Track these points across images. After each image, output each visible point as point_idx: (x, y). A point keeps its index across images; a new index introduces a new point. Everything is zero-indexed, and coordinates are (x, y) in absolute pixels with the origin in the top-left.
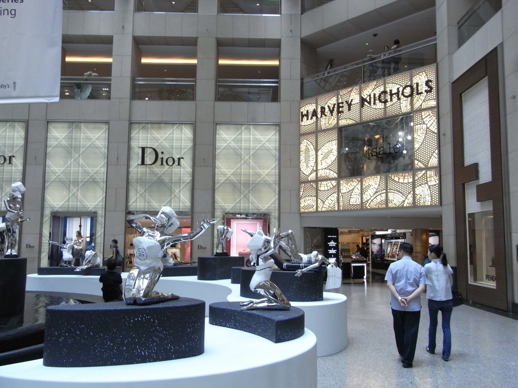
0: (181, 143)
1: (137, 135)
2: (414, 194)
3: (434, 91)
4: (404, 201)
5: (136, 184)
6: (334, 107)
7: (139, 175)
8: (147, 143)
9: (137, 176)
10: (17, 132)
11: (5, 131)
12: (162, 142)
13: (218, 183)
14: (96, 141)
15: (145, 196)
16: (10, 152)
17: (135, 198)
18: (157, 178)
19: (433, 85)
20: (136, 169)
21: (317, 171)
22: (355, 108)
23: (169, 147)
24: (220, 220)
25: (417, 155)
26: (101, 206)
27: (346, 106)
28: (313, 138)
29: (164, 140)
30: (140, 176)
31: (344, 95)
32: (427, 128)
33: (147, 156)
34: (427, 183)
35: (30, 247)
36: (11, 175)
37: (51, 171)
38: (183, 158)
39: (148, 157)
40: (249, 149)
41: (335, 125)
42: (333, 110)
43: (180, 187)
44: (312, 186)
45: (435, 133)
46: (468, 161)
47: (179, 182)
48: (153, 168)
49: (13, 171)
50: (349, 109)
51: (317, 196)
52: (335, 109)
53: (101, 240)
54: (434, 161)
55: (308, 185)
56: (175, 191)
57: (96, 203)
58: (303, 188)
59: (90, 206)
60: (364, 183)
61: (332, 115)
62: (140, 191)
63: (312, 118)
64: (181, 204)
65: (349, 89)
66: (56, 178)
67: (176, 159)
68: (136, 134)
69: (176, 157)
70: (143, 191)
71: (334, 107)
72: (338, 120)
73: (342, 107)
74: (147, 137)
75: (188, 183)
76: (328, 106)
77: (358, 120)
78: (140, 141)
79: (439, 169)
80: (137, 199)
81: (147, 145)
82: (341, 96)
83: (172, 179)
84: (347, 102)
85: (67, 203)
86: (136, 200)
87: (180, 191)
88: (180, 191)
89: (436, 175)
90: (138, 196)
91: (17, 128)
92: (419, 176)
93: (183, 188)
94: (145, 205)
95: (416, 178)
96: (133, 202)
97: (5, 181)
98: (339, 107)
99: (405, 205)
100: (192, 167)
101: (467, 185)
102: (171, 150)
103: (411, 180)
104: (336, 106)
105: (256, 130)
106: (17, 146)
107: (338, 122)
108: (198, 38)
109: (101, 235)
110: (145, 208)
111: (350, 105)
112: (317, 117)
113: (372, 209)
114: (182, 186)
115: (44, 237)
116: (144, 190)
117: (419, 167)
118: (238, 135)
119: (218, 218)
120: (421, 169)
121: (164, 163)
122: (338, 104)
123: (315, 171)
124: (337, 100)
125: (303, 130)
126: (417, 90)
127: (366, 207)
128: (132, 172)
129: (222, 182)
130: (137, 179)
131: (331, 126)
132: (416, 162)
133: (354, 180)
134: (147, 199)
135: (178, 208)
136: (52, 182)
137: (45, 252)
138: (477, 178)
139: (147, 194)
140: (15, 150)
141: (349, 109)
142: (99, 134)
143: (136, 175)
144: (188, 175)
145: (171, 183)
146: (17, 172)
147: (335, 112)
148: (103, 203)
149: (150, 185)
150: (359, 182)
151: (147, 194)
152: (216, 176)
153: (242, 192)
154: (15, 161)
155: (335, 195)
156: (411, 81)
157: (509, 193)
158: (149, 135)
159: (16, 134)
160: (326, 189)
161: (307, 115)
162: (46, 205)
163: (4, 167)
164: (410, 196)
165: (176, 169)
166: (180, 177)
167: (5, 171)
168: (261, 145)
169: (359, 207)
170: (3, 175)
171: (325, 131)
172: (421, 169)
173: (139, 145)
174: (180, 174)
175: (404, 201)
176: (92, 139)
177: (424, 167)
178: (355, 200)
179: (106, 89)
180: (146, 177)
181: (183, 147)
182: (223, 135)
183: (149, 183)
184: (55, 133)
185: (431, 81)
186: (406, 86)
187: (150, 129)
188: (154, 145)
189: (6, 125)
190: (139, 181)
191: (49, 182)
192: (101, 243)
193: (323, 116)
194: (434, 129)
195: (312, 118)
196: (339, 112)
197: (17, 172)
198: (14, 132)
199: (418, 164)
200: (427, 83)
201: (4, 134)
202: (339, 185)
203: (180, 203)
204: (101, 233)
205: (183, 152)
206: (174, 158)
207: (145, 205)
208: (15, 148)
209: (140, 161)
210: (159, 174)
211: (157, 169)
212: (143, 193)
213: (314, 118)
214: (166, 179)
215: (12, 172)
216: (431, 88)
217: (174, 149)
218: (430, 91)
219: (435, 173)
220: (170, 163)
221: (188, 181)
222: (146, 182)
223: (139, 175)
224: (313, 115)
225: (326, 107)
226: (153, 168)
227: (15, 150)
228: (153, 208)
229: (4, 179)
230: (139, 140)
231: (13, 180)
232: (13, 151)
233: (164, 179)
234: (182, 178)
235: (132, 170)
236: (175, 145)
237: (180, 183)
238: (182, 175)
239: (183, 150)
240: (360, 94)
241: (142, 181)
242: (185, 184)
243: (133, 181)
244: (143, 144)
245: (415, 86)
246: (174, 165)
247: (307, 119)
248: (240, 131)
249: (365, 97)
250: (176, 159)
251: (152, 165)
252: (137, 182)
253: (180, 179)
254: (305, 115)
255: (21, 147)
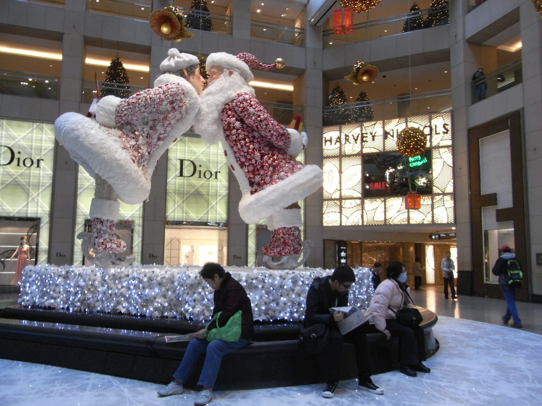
0: (218, 158)
1: (175, 147)
2: (433, 214)
3: (450, 133)
4: (424, 220)
5: (174, 195)
6: (358, 137)
7: (177, 186)
8: (185, 155)
9: (175, 187)
10: (45, 134)
11: (32, 132)
12: (199, 156)
13: (81, 188)
14: (21, 141)
15: (183, 207)
16: (38, 155)
17: (173, 209)
18: (194, 190)
19: (449, 127)
20: (174, 180)
21: (340, 190)
22: (379, 139)
23: (206, 161)
24: (82, 226)
25: (435, 183)
26: (138, 216)
27: (370, 137)
28: (336, 162)
29: (201, 154)
30: (178, 188)
31: (368, 127)
32: (444, 162)
33: (185, 168)
34: (444, 205)
35: (60, 255)
36: (39, 179)
37: (84, 178)
38: (43, 160)
39: (186, 169)
40: (217, 163)
41: (359, 152)
42: (357, 139)
43: (217, 199)
44: (336, 203)
45: (451, 167)
46: (486, 190)
47: (216, 195)
48: (190, 180)
49: (41, 175)
50: (373, 140)
51: (341, 212)
52: (359, 138)
53: (138, 249)
54: (450, 189)
55: (331, 202)
56: (32, 195)
57: (133, 212)
58: (326, 205)
59: (127, 215)
60: (387, 203)
61: (356, 143)
62: (178, 201)
63: (335, 144)
64: (39, 209)
65: (374, 123)
66: (89, 185)
67: (35, 161)
68: (173, 146)
69: (213, 171)
70: (181, 202)
71: (358, 137)
72: (362, 147)
73: (366, 137)
74: (185, 150)
75: (224, 196)
76: (353, 135)
77: (381, 149)
78: (178, 153)
79: (454, 195)
80: (175, 209)
81: (185, 157)
82: (365, 127)
83: (209, 192)
84: (371, 134)
85: (25, 208)
86: (174, 210)
87: (216, 204)
88: (216, 204)
89: (452, 200)
90: (176, 206)
91: (46, 130)
92: (437, 200)
93: (219, 201)
94: (183, 216)
95: (434, 201)
96: (171, 213)
97: (32, 185)
98: (363, 137)
99: (425, 223)
100: (52, 169)
101: (483, 209)
102: (208, 163)
103: (430, 203)
104: (360, 136)
105: (10, 125)
106: (45, 149)
107: (362, 150)
108: (63, 33)
109: (138, 244)
110: (183, 219)
111: (373, 137)
112: (341, 143)
113: (394, 225)
114: (41, 190)
115: (77, 246)
116: (182, 200)
117: (437, 192)
118: (29, 133)
119: (80, 224)
120: (438, 194)
121: (202, 175)
122: (362, 134)
123: (338, 190)
124: (362, 131)
125: (326, 153)
126: (436, 131)
127: (390, 224)
128: (170, 183)
129: (7, 183)
130: (175, 190)
131: (355, 153)
132: (434, 188)
133: (378, 200)
134: (185, 210)
135: (36, 212)
136: (85, 189)
137: (78, 261)
138: (496, 204)
139: (184, 205)
140: (43, 153)
141: (373, 140)
142: (25, 134)
143: (174, 186)
144: (224, 189)
145: (208, 195)
146: (45, 177)
147: (359, 141)
148: (140, 212)
149: (188, 195)
150: (382, 202)
151: (184, 205)
152: (79, 180)
153: (176, 202)
154: (44, 165)
155: (360, 212)
156: (430, 122)
157: (528, 217)
158: (187, 148)
159: (44, 136)
160: (351, 206)
161: (331, 141)
162: (79, 212)
163: (30, 170)
164: (430, 215)
165: (34, 171)
166: (217, 190)
167: (32, 175)
168: (14, 142)
169: (383, 223)
170: (30, 179)
171: (349, 156)
172: (438, 194)
173: (176, 157)
174: (217, 187)
175: (424, 220)
176: (197, 153)
177: (441, 192)
178: (379, 218)
179: (24, 83)
180: (184, 188)
181: (43, 148)
182: (11, 132)
183: (187, 194)
184: (11, 132)
185: (447, 125)
186: (426, 127)
187: (188, 142)
188: (192, 158)
189: (33, 126)
190: (177, 192)
191: (82, 189)
192: (138, 252)
193: (347, 143)
194: (450, 162)
195: (335, 144)
196: (362, 141)
197: (45, 177)
198: (42, 134)
199: (435, 190)
200: (444, 126)
201: (30, 135)
202: (363, 203)
203: (216, 215)
204: (139, 243)
205: (219, 167)
206: (33, 159)
207: (183, 216)
208: (43, 150)
209: (178, 173)
210: (196, 186)
211: (195, 181)
212: (181, 204)
213: (338, 144)
214: (204, 191)
215: (39, 177)
216: (448, 130)
217: (211, 163)
218: (447, 133)
219: (451, 198)
220: (208, 175)
221: (224, 194)
222: (184, 194)
223: (177, 186)
224: (337, 141)
225: (350, 135)
226: (190, 180)
227: (43, 153)
228: (190, 219)
229: (31, 184)
230: (176, 151)
231: (41, 184)
232: (41, 154)
233: (201, 191)
234: (218, 191)
235: (170, 181)
236: (35, 145)
237: (217, 195)
238: (218, 189)
239: (219, 164)
240: (384, 127)
241: (180, 193)
242: (221, 196)
243: (171, 191)
244: (180, 156)
245: (433, 127)
246: (32, 167)
247: (331, 144)
248: (31, 129)
249: (388, 131)
250: (35, 161)
251: (8, 166)
252: (175, 193)
253: (217, 192)
254: (328, 140)
255: (50, 150)
